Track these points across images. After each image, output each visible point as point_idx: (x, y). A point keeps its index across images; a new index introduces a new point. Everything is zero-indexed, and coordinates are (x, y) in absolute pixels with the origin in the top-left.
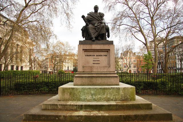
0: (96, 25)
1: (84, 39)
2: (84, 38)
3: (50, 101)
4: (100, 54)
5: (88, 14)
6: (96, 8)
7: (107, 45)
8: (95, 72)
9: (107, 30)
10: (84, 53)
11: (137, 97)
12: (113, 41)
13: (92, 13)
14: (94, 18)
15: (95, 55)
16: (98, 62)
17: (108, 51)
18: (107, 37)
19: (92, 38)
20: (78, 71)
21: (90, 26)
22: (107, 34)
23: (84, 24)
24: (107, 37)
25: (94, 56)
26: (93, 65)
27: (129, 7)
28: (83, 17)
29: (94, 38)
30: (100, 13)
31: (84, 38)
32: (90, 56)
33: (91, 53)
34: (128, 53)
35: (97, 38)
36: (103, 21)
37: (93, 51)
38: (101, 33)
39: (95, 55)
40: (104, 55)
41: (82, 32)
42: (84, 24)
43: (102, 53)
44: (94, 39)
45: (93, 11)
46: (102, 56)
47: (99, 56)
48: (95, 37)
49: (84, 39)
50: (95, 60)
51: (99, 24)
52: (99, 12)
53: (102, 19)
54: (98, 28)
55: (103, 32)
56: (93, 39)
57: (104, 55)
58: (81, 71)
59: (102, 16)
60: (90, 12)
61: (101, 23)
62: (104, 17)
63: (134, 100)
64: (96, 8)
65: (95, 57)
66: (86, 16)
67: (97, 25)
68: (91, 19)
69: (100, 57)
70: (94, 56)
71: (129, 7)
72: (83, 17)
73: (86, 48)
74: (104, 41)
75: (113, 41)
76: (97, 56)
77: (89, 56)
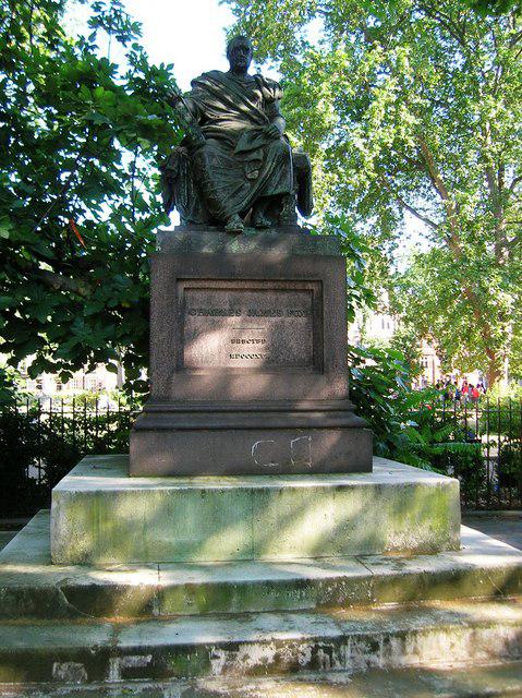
45: (224, 66)
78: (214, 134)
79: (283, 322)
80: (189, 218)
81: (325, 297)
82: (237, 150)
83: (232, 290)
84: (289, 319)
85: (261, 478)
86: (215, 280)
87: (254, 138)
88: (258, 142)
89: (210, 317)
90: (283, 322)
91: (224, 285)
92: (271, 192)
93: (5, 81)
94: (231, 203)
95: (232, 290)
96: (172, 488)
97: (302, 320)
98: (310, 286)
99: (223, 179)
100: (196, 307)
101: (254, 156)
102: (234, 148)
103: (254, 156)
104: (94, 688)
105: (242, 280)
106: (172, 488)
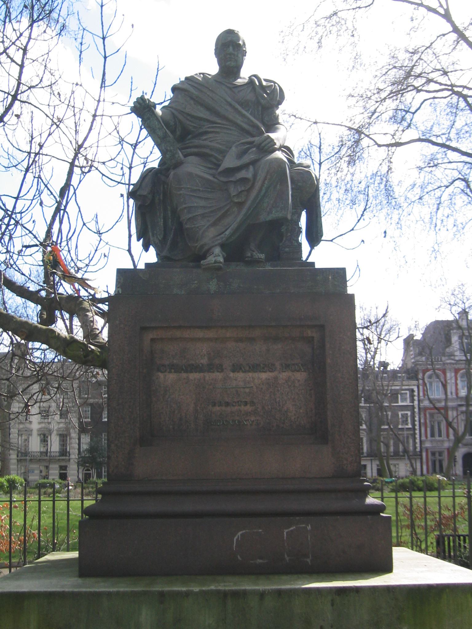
0: (229, 162)
2: (152, 249)
3: (205, 140)
6: (230, 48)
9: (306, 194)
10: (76, 521)
12: (345, 268)
18: (303, 239)
21: (193, 167)
22: (303, 222)
23: (150, 155)
24: (303, 239)
27: (456, 30)
28: (143, 108)
29: (217, 250)
31: (152, 249)
34: (455, 339)
36: (276, 136)
42: (150, 155)
44: (217, 256)
45: (211, 67)
49: (151, 256)
51: (246, 159)
52: (245, 73)
53: (272, 124)
54: (244, 180)
56: (211, 259)
59: (264, 101)
61: (270, 146)
62: (282, 112)
64: (230, 48)
66: (161, 97)
67: (238, 163)
71: (456, 30)
72: (143, 108)
75: (345, 268)
78: (195, 150)
79: (276, 378)
80: (164, 253)
81: (328, 346)
82: (221, 169)
83: (209, 340)
84: (284, 375)
85: (284, 577)
86: (189, 327)
87: (245, 152)
88: (250, 157)
89: (184, 375)
90: (276, 378)
91: (200, 334)
92: (264, 217)
93: (2, 224)
94: (212, 232)
95: (209, 340)
96: (244, 112)
97: (301, 376)
98: (309, 333)
99: (202, 203)
100: (167, 363)
101: (243, 174)
102: (219, 166)
103: (243, 174)
104: (217, 408)
105: (222, 327)
106: (244, 112)
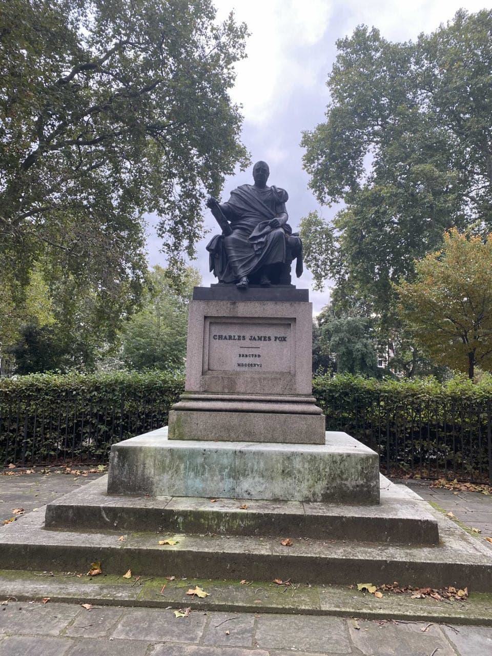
0: (255, 233)
1: (216, 281)
4: (262, 334)
5: (232, 193)
7: (287, 305)
8: (194, 523)
11: (388, 487)
12: (308, 290)
13: (246, 189)
14: (252, 207)
15: (248, 336)
16: (257, 361)
17: (288, 322)
19: (238, 280)
20: (186, 389)
25: (244, 338)
26: (238, 369)
29: (245, 279)
30: (274, 190)
32: (230, 338)
33: (234, 331)
35: (255, 279)
37: (279, 322)
38: (270, 262)
39: (248, 336)
40: (276, 338)
41: (211, 255)
43: (271, 332)
46: (270, 339)
47: (260, 339)
48: (248, 276)
50: (246, 351)
52: (269, 184)
55: (279, 259)
57: (276, 338)
58: (196, 389)
60: (241, 184)
63: (370, 496)
65: (247, 343)
68: (241, 212)
69: (261, 344)
70: (244, 338)
73: (215, 314)
74: (278, 290)
75: (308, 290)
76: (253, 339)
77: (225, 338)
